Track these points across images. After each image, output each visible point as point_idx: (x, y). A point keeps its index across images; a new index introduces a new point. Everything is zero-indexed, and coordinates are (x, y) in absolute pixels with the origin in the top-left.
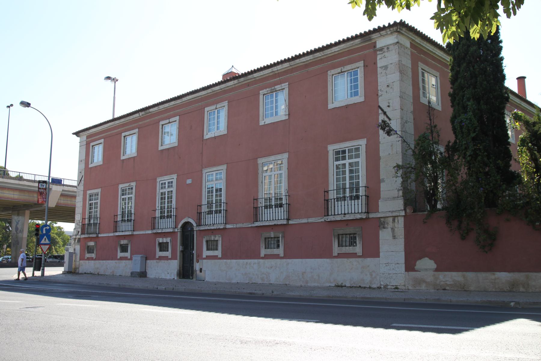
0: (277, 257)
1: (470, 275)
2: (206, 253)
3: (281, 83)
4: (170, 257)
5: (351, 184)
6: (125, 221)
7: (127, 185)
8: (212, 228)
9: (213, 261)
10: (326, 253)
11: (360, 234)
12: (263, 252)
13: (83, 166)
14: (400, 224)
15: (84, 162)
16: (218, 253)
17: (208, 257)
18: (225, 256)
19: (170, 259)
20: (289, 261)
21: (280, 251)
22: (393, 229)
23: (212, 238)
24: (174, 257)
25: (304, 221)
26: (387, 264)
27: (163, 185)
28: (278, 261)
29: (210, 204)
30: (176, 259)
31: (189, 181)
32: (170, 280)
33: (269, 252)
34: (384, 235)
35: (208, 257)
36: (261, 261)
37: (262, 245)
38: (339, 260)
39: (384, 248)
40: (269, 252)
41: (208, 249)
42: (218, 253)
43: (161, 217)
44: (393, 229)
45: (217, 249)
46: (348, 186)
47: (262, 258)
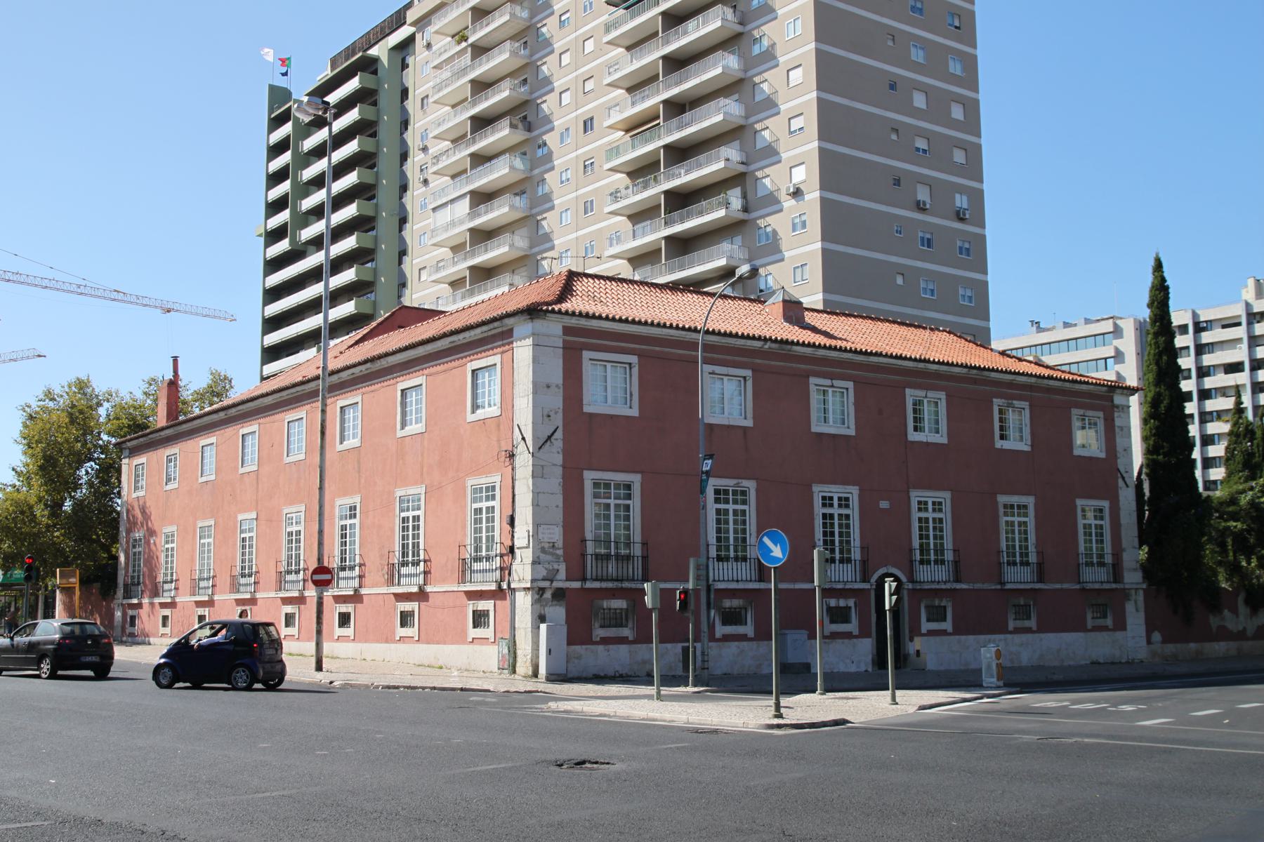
0: (1028, 630)
1: (1179, 645)
2: (926, 626)
3: (1020, 398)
4: (856, 632)
5: (935, 544)
6: (1092, 564)
7: (732, 482)
8: (943, 587)
9: (938, 638)
10: (1080, 626)
11: (1107, 604)
12: (1011, 625)
13: (556, 401)
14: (1141, 597)
15: (1119, 449)
16: (947, 625)
17: (931, 633)
18: (958, 630)
19: (856, 637)
20: (1043, 635)
21: (1032, 623)
22: (1136, 602)
23: (937, 603)
24: (864, 633)
25: (1058, 586)
26: (1133, 637)
27: (827, 502)
28: (1030, 636)
29: (924, 549)
30: (868, 636)
31: (884, 504)
32: (857, 674)
33: (1019, 624)
34: (1130, 607)
35: (931, 633)
36: (1009, 636)
37: (1011, 617)
38: (1093, 634)
39: (1130, 621)
40: (1019, 624)
41: (929, 620)
42: (947, 625)
43: (922, 562)
44: (1136, 602)
45: (944, 620)
46: (932, 546)
47: (1011, 633)
